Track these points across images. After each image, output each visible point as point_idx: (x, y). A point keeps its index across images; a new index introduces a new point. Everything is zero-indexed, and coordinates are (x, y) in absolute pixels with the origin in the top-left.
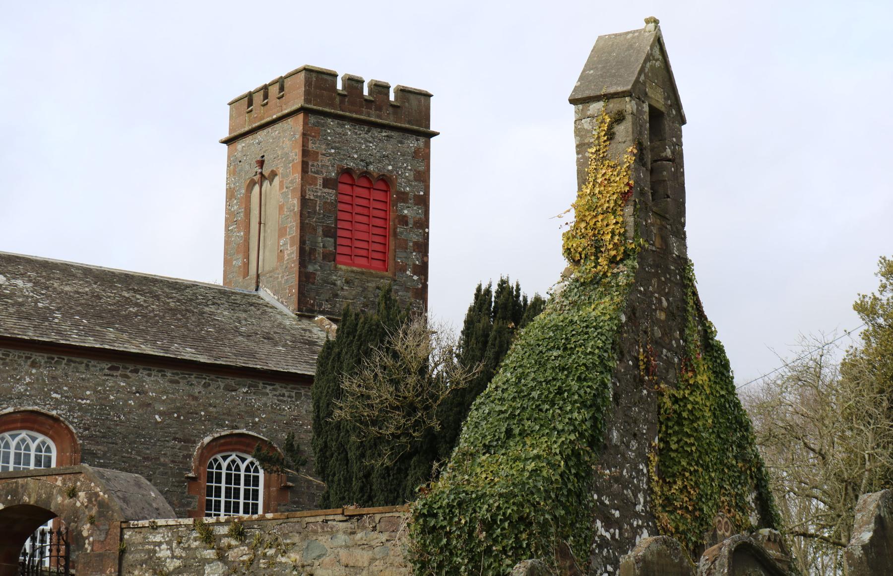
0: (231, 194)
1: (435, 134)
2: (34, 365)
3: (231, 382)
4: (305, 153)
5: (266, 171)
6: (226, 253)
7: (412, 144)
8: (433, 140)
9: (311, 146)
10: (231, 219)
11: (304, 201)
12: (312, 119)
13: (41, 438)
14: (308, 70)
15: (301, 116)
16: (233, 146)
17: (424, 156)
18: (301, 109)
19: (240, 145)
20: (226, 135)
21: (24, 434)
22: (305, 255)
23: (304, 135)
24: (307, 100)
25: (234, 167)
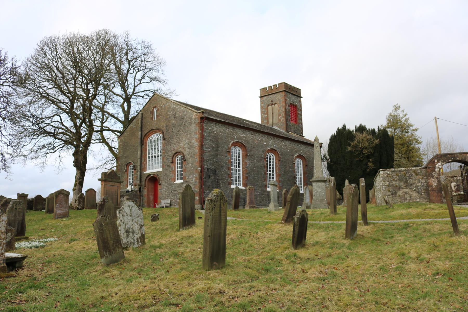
0: (262, 108)
1: (302, 97)
2: (271, 139)
3: (298, 144)
4: (285, 99)
5: (274, 103)
6: (261, 119)
7: (299, 99)
8: (302, 98)
9: (286, 98)
10: (262, 113)
11: (286, 109)
12: (286, 93)
13: (272, 154)
14: (285, 83)
15: (284, 92)
16: (262, 98)
17: (300, 101)
18: (285, 91)
19: (264, 98)
20: (260, 96)
21: (270, 154)
22: (286, 120)
23: (285, 96)
24: (285, 88)
25: (262, 102)
